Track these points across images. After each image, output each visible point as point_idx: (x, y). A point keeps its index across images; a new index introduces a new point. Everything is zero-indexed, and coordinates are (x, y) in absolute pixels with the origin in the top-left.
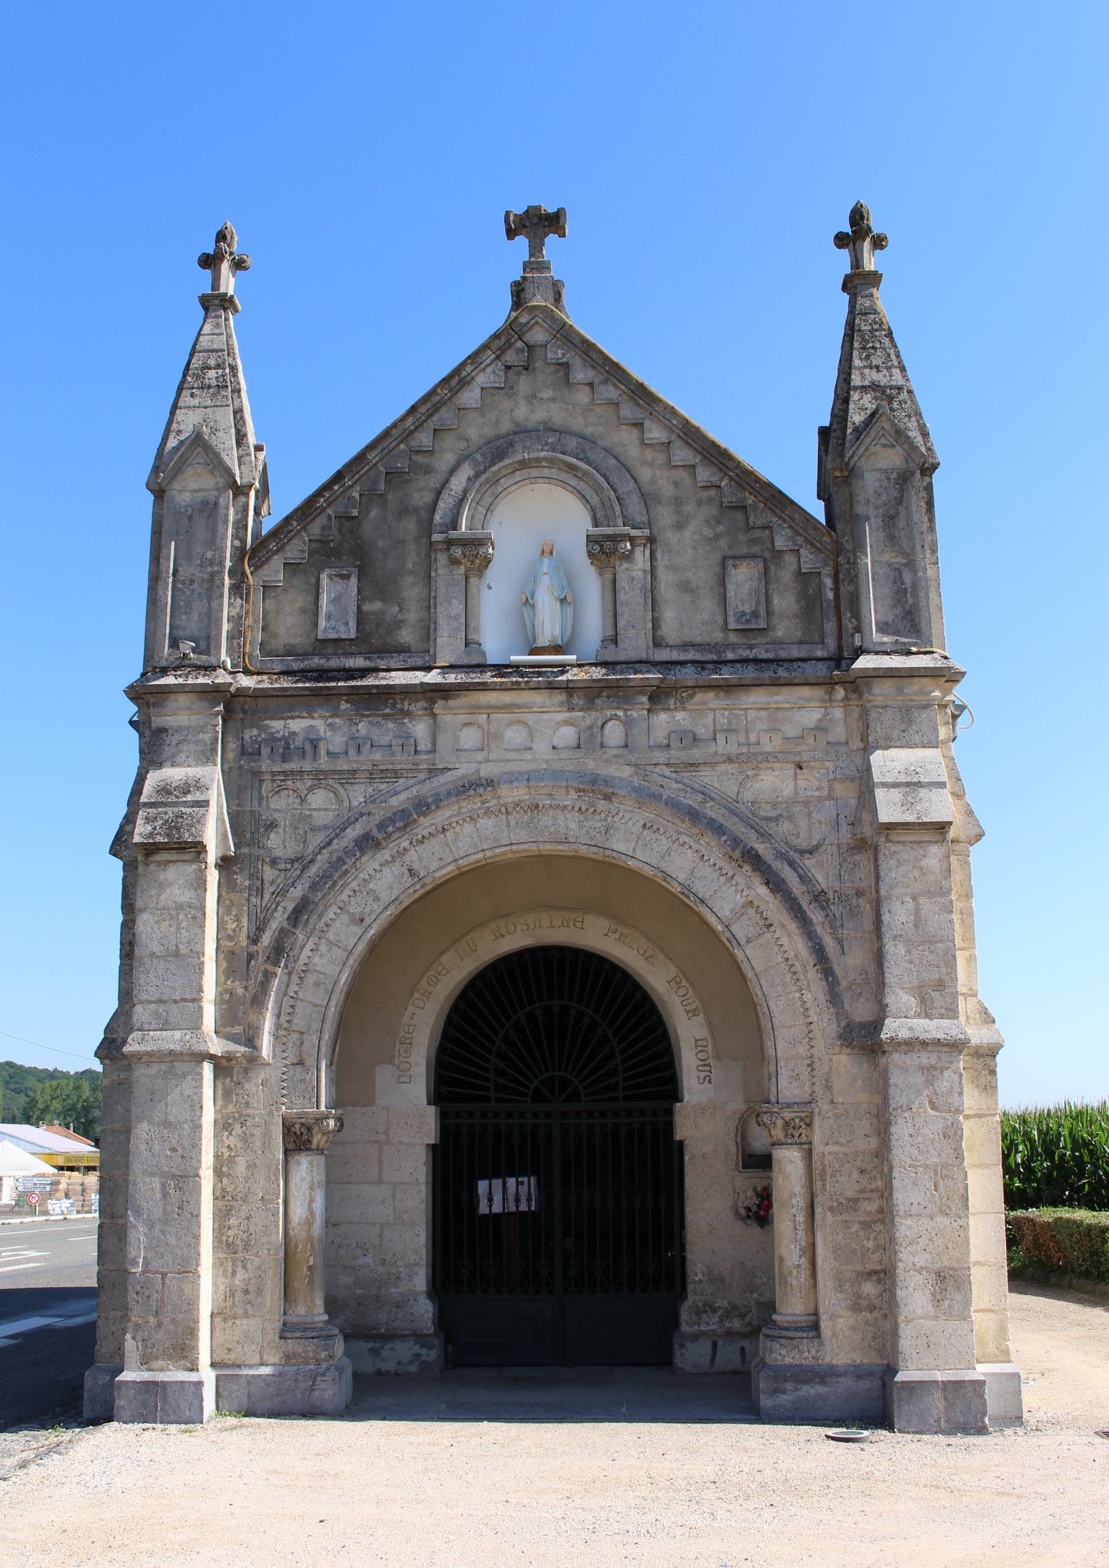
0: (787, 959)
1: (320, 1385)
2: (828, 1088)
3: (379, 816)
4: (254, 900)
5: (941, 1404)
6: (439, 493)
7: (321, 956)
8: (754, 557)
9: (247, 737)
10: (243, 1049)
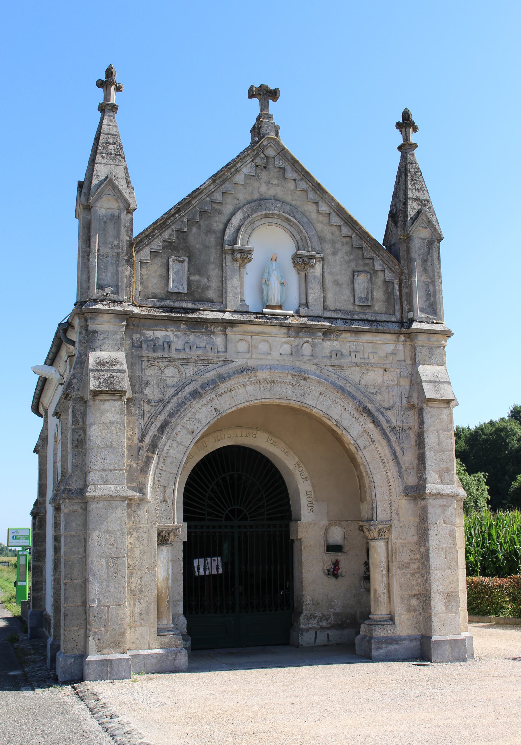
0: (381, 457)
1: (179, 657)
2: (398, 514)
3: (201, 381)
4: (140, 420)
5: (449, 650)
6: (226, 225)
7: (174, 449)
8: (366, 272)
9: (134, 338)
10: (138, 494)
